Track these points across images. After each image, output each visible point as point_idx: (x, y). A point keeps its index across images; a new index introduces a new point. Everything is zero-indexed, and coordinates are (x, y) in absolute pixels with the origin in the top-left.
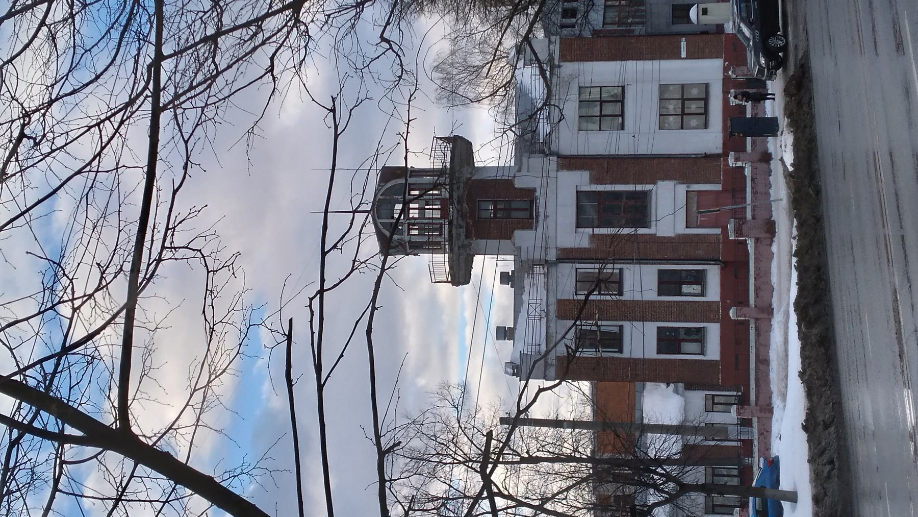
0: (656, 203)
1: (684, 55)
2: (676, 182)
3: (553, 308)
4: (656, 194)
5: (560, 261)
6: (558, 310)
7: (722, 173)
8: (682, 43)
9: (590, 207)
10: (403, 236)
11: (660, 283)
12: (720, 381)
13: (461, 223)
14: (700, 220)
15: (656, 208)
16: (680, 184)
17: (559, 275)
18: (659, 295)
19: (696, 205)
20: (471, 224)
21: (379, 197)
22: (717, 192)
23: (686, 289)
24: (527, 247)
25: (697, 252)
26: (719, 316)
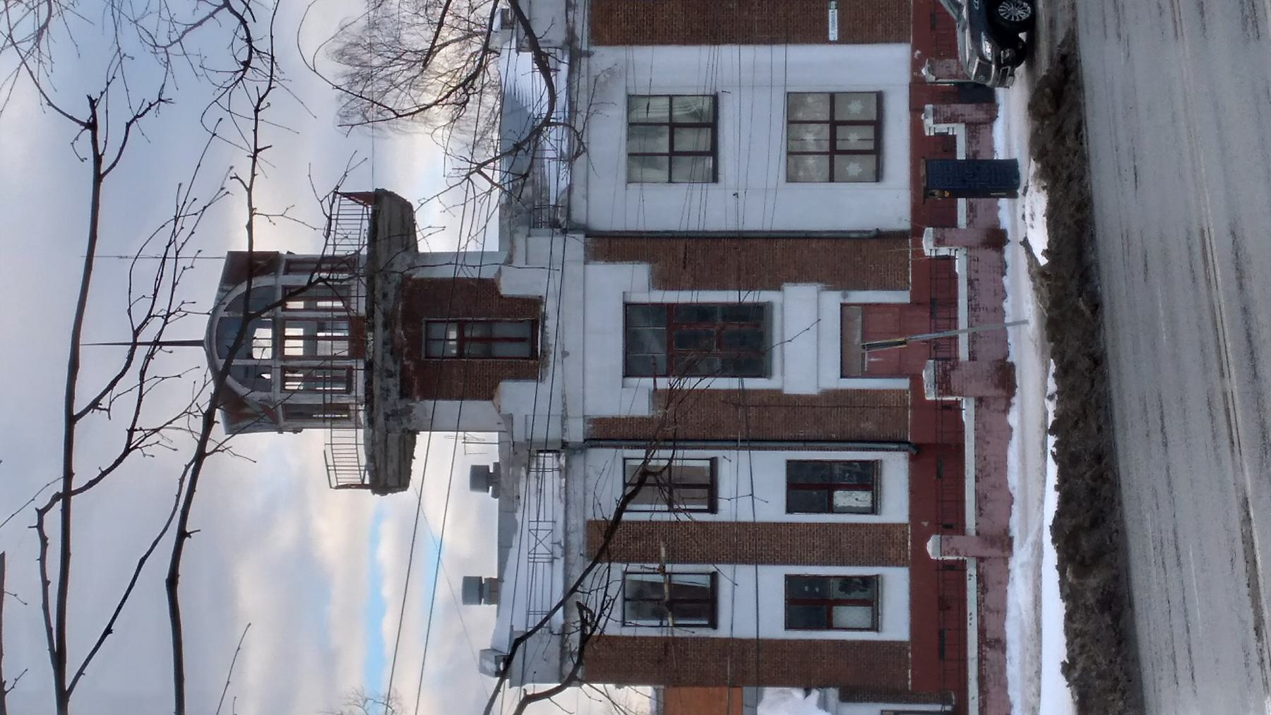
0: (783, 319)
1: (833, 34)
2: (820, 286)
3: (577, 539)
4: (782, 308)
5: (594, 443)
7: (910, 269)
8: (830, 11)
9: (656, 348)
10: (271, 394)
11: (792, 486)
12: (910, 683)
13: (390, 365)
14: (869, 362)
18: (790, 510)
19: (859, 333)
20: (411, 368)
21: (222, 313)
22: (901, 307)
23: (841, 498)
24: (526, 416)
26: (907, 555)
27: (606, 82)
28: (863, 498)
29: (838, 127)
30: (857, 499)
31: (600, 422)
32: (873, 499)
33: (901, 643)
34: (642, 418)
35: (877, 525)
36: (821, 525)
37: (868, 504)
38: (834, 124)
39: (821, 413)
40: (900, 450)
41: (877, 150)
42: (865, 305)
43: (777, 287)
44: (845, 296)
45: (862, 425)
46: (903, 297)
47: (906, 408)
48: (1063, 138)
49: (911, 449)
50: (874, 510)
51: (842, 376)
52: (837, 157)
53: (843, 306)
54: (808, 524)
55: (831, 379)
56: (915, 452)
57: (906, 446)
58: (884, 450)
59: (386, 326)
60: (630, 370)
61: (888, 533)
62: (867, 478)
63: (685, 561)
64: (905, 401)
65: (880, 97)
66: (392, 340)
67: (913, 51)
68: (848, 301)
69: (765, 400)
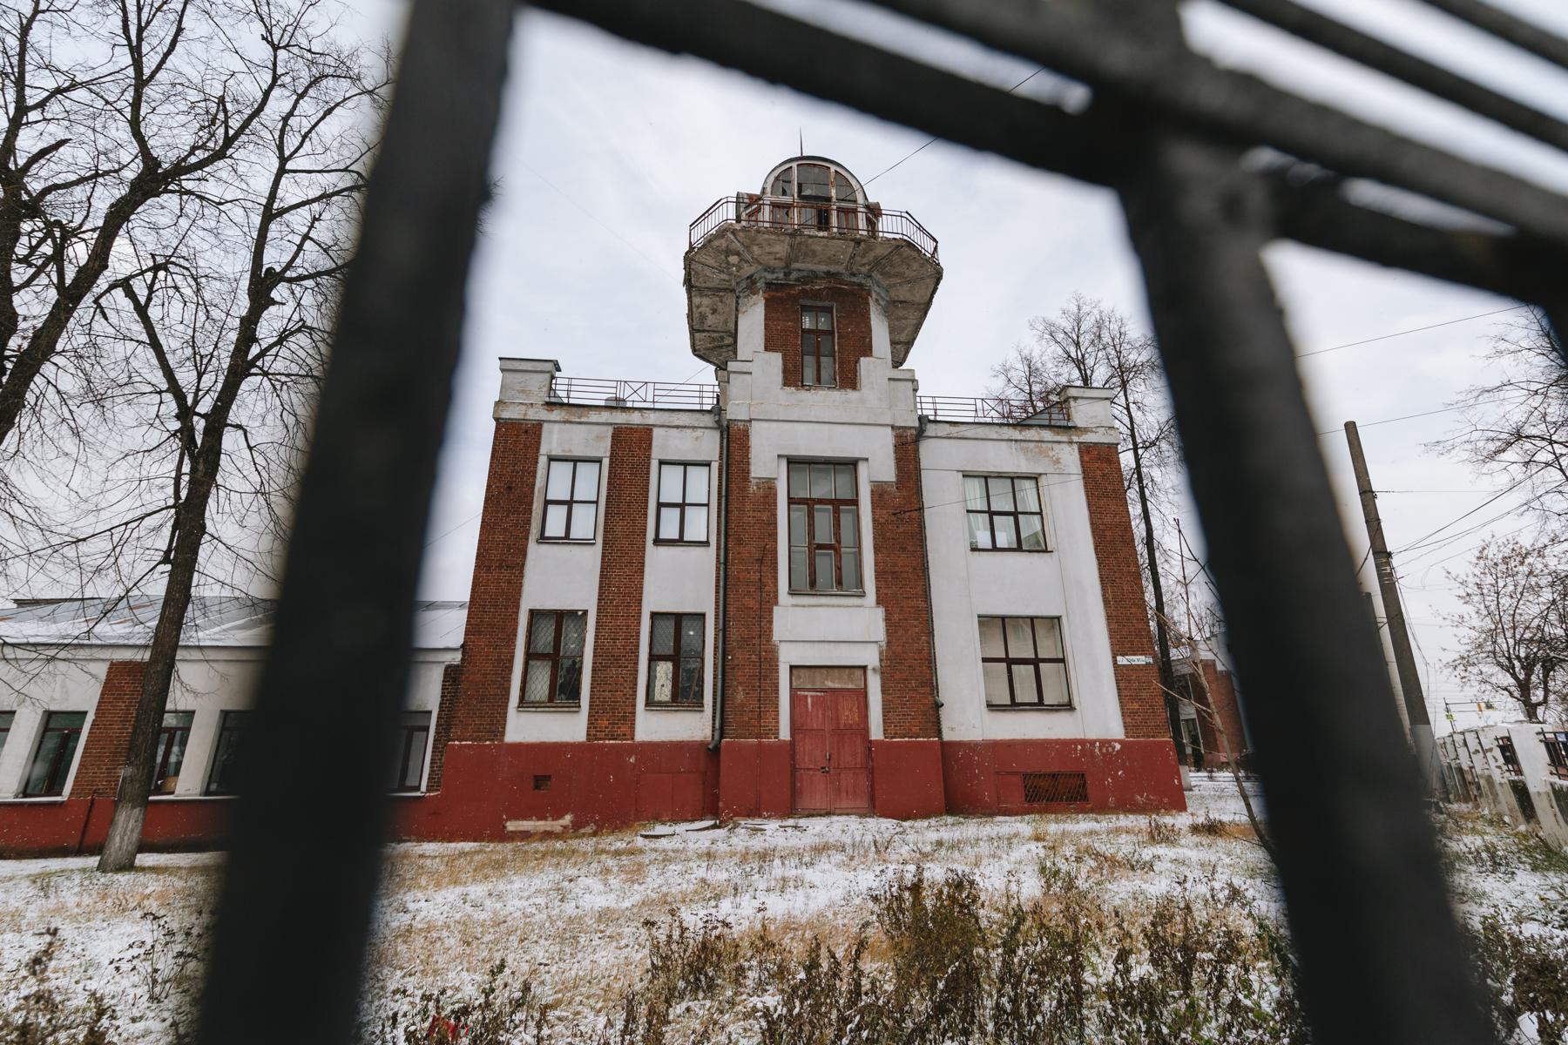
0: (833, 606)
1: (1121, 660)
2: (884, 644)
6: (631, 429)
7: (906, 739)
13: (794, 275)
14: (806, 696)
16: (881, 653)
17: (699, 432)
18: (654, 615)
19: (837, 686)
22: (865, 730)
23: (664, 670)
25: (740, 688)
26: (601, 739)
27: (1048, 456)
28: (663, 692)
29: (1032, 667)
30: (663, 686)
31: (745, 436)
32: (1035, 426)
33: (503, 734)
34: (748, 472)
35: (634, 706)
36: (637, 646)
37: (657, 697)
38: (1035, 662)
39: (754, 645)
40: (713, 731)
41: (1014, 706)
42: (866, 693)
43: (880, 601)
44: (874, 669)
45: (740, 688)
46: (876, 732)
47: (759, 736)
48: (1097, 923)
49: (714, 742)
50: (650, 703)
51: (792, 667)
52: (1004, 665)
53: (864, 668)
54: (638, 634)
55: (788, 656)
56: (710, 747)
57: (717, 737)
58: (714, 713)
59: (828, 273)
60: (795, 463)
61: (624, 718)
62: (685, 695)
63: (607, 514)
64: (767, 736)
65: (1068, 706)
66: (817, 277)
67: (1120, 742)
68: (870, 673)
69: (767, 588)
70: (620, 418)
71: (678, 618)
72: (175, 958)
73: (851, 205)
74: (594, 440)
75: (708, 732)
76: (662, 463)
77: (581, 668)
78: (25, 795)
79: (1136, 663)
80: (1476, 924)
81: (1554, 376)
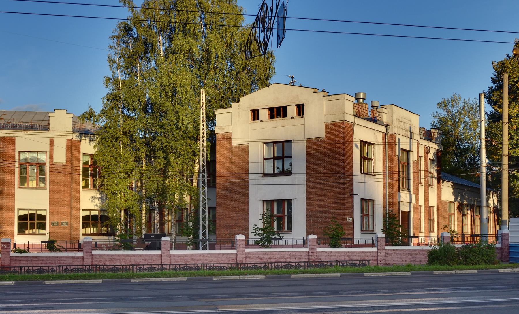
1: (275, 109)
15: (282, 281)
70: (505, 214)
71: (281, 202)
72: (178, 6)
73: (14, 162)
74: (286, 166)
75: (236, 237)
76: (19, 152)
77: (120, 250)
78: (402, 212)
79: (204, 101)
80: (96, 150)
81: (116, 34)
